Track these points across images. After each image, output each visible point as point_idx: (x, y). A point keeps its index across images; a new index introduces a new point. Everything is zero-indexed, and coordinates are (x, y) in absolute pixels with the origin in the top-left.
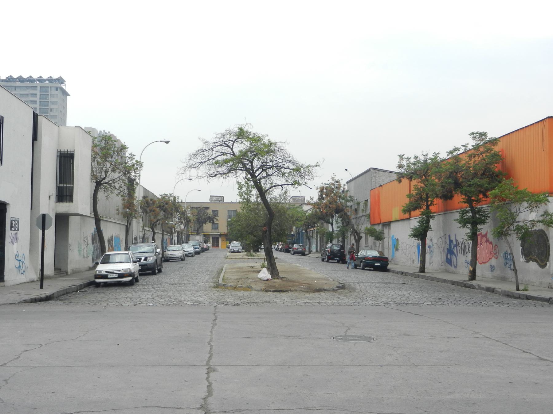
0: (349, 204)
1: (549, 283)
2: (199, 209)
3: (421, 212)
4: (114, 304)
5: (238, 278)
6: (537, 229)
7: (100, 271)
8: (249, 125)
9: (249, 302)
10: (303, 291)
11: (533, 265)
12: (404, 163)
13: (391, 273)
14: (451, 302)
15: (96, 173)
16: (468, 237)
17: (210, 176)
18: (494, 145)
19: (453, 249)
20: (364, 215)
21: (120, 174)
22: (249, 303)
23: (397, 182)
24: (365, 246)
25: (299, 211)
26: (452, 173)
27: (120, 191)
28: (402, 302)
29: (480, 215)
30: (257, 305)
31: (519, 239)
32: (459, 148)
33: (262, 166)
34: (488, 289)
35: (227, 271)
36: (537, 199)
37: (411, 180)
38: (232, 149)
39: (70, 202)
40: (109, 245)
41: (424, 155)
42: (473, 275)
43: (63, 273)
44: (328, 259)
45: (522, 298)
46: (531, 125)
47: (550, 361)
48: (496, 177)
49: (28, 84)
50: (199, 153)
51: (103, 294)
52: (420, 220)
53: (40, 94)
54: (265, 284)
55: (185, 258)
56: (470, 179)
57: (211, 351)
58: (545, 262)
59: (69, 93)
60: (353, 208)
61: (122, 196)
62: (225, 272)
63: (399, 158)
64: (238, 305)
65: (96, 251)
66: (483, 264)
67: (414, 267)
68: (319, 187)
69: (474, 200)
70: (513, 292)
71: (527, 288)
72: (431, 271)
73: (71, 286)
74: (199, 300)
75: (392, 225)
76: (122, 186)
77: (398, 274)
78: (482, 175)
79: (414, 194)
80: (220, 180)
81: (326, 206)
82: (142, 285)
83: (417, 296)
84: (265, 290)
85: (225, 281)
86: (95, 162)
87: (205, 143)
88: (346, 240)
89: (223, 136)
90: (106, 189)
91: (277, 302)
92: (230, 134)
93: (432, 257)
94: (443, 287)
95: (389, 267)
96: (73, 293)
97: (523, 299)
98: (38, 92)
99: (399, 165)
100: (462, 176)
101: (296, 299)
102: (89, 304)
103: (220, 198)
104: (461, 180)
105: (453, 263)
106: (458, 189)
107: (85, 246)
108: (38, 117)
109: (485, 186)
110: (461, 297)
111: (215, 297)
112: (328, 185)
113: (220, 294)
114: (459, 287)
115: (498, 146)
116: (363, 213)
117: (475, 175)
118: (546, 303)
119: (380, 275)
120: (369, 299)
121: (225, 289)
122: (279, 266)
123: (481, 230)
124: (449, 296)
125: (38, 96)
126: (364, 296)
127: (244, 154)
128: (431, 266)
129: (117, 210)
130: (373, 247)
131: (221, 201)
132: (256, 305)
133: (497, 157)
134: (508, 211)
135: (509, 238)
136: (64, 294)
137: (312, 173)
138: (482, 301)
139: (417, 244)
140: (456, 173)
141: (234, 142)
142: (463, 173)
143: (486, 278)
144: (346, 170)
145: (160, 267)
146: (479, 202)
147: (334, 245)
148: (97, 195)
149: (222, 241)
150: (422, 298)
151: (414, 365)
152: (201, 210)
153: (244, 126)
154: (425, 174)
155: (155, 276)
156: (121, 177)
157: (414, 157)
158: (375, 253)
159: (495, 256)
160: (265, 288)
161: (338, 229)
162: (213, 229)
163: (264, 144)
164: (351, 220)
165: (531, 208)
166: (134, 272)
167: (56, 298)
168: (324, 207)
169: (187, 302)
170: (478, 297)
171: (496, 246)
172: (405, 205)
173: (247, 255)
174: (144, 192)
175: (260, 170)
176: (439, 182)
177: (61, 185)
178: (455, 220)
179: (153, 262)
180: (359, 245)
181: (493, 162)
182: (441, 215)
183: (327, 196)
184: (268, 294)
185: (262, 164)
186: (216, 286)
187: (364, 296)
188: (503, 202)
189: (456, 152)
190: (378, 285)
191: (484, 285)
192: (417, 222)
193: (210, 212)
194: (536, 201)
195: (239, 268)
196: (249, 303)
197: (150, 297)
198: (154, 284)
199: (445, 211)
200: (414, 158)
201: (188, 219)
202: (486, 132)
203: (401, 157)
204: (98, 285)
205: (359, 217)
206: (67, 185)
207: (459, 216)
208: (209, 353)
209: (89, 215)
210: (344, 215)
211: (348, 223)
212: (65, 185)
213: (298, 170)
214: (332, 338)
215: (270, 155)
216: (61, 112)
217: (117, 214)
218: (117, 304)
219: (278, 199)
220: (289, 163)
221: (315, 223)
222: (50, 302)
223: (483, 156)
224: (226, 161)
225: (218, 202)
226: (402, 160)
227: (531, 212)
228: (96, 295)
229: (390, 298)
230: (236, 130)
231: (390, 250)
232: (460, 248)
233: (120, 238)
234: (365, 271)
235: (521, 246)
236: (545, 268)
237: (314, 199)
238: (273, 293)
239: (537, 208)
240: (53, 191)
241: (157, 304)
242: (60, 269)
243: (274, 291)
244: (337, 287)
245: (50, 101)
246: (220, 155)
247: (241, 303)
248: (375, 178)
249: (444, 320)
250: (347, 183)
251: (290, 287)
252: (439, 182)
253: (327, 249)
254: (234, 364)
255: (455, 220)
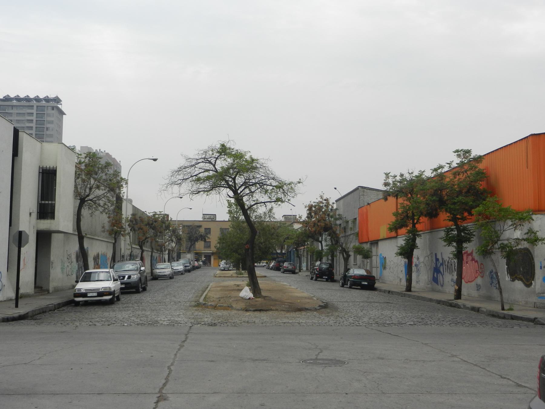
0: (338, 222)
1: (535, 303)
2: (191, 227)
3: (407, 230)
4: (87, 324)
5: (220, 297)
6: (522, 248)
7: (80, 290)
8: (232, 142)
9: (227, 321)
10: (284, 311)
11: (519, 285)
12: (390, 181)
13: (378, 292)
14: (434, 322)
15: (81, 190)
16: (453, 256)
17: (193, 193)
18: (478, 163)
19: (439, 268)
20: (353, 234)
21: (105, 191)
22: (226, 323)
23: (383, 200)
24: (354, 265)
25: (290, 229)
26: (436, 190)
27: (105, 208)
28: (384, 322)
29: (465, 233)
30: (235, 325)
31: (504, 257)
32: (444, 166)
33: (245, 183)
34: (473, 309)
35: (212, 289)
36: (521, 216)
37: (397, 199)
38: (214, 166)
39: (51, 219)
40: (95, 263)
41: (410, 173)
42: (458, 294)
43: (44, 291)
44: (317, 277)
45: (507, 318)
46: (514, 143)
47: (528, 388)
48: (481, 195)
49: (24, 103)
50: (181, 169)
51: (79, 313)
52: (407, 238)
53: (37, 114)
54: (246, 303)
55: (173, 276)
56: (455, 197)
57: (168, 377)
58: (531, 281)
59: (65, 112)
60: (342, 226)
61: (106, 213)
62: (209, 290)
63: (385, 176)
64: (215, 325)
65: (81, 269)
66: (469, 283)
67: (402, 286)
68: (307, 205)
69: (459, 219)
70: (498, 311)
71: (512, 308)
72: (418, 290)
73: (48, 305)
74: (176, 319)
75: (380, 244)
76: (107, 203)
77: (384, 292)
78: (466, 193)
79: (400, 212)
80: (202, 197)
81: (315, 224)
82: (122, 303)
83: (400, 315)
84: (245, 309)
85: (207, 299)
86: (80, 179)
87: (188, 159)
88: (335, 258)
89: (206, 152)
90: (91, 206)
91: (256, 322)
92: (212, 150)
93: (419, 275)
94: (429, 306)
95: (377, 285)
96: (50, 312)
97: (508, 319)
98: (34, 111)
99: (385, 183)
100: (446, 194)
101: (276, 318)
102: (61, 323)
103: (212, 217)
104: (445, 198)
105: (440, 282)
106: (442, 206)
107: (68, 264)
108: (20, 133)
109: (470, 204)
110: (444, 317)
111: (193, 316)
112: (317, 203)
113: (199, 313)
114: (445, 306)
115: (482, 164)
116: (352, 232)
117: (460, 193)
118: (531, 324)
119: (366, 293)
120: (350, 319)
121: (206, 308)
122: (262, 283)
123: (467, 249)
124: (433, 316)
125: (35, 115)
126: (346, 316)
127: (226, 171)
128: (418, 284)
129: (103, 227)
130: (362, 266)
131: (213, 220)
132: (234, 325)
133: (482, 175)
134: (493, 230)
135: (493, 257)
136: (40, 313)
137: (295, 190)
138: (465, 321)
139: (404, 263)
140: (441, 191)
141: (217, 158)
142: (448, 191)
143: (472, 297)
144: (335, 188)
145: (144, 285)
146: (464, 221)
147: (322, 263)
148: (81, 212)
149: (214, 259)
150: (404, 318)
151: (383, 392)
152: (193, 228)
153: (227, 142)
154: (411, 191)
155: (139, 294)
156: (105, 194)
157: (399, 175)
158: (362, 272)
159: (481, 274)
160: (245, 307)
161: (327, 248)
162: (205, 247)
163: (246, 161)
164: (340, 238)
165: (515, 226)
166: (114, 290)
167: (31, 317)
168: (312, 225)
169: (163, 322)
170: (462, 317)
171: (482, 265)
172: (391, 223)
173: (236, 273)
174: (133, 209)
175: (243, 187)
176: (424, 200)
177: (42, 202)
178: (440, 238)
179: (137, 280)
180: (348, 264)
181: (478, 180)
182: (427, 234)
183: (315, 214)
184: (248, 314)
185: (245, 181)
186: (197, 305)
187: (346, 316)
188: (487, 220)
189: (441, 169)
190: (362, 304)
191: (469, 304)
192: (403, 240)
193: (202, 230)
194: (520, 219)
195: (224, 287)
196: (226, 323)
197: (127, 316)
198: (135, 303)
199: (431, 229)
200: (400, 176)
201: (179, 237)
202: (471, 150)
203: (387, 175)
204: (77, 304)
205: (348, 235)
206: (46, 202)
207: (444, 234)
208: (165, 379)
209: (72, 232)
210: (332, 233)
211: (337, 242)
212: (47, 202)
213: (280, 187)
214: (301, 362)
215: (252, 172)
216: (56, 130)
217: (103, 232)
218: (91, 323)
219: (263, 216)
220: (272, 180)
221: (305, 241)
222: (22, 321)
223: (467, 174)
224: (208, 178)
225: (210, 220)
226: (388, 178)
227: (515, 229)
228: (72, 314)
229: (372, 317)
230: (218, 146)
231: (378, 268)
232: (446, 266)
233: (107, 256)
234: (352, 290)
235: (507, 265)
236: (531, 287)
237: (302, 217)
238: (253, 313)
239: (522, 226)
240: (33, 207)
241: (131, 324)
242: (41, 288)
243: (255, 311)
244: (320, 306)
245: (46, 121)
246: (202, 172)
247: (219, 323)
248: (364, 197)
249: (423, 342)
250: (336, 201)
251: (271, 306)
252: (424, 200)
253: (315, 268)
254: (188, 392)
255: (440, 238)
